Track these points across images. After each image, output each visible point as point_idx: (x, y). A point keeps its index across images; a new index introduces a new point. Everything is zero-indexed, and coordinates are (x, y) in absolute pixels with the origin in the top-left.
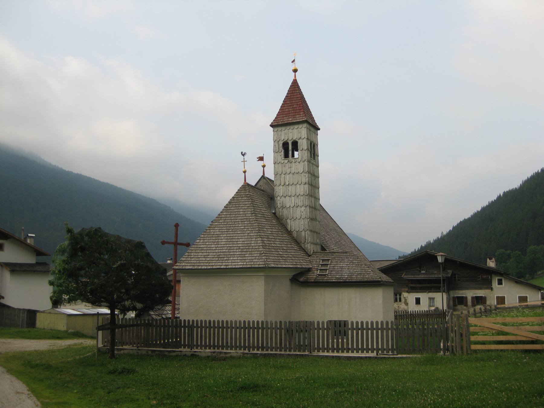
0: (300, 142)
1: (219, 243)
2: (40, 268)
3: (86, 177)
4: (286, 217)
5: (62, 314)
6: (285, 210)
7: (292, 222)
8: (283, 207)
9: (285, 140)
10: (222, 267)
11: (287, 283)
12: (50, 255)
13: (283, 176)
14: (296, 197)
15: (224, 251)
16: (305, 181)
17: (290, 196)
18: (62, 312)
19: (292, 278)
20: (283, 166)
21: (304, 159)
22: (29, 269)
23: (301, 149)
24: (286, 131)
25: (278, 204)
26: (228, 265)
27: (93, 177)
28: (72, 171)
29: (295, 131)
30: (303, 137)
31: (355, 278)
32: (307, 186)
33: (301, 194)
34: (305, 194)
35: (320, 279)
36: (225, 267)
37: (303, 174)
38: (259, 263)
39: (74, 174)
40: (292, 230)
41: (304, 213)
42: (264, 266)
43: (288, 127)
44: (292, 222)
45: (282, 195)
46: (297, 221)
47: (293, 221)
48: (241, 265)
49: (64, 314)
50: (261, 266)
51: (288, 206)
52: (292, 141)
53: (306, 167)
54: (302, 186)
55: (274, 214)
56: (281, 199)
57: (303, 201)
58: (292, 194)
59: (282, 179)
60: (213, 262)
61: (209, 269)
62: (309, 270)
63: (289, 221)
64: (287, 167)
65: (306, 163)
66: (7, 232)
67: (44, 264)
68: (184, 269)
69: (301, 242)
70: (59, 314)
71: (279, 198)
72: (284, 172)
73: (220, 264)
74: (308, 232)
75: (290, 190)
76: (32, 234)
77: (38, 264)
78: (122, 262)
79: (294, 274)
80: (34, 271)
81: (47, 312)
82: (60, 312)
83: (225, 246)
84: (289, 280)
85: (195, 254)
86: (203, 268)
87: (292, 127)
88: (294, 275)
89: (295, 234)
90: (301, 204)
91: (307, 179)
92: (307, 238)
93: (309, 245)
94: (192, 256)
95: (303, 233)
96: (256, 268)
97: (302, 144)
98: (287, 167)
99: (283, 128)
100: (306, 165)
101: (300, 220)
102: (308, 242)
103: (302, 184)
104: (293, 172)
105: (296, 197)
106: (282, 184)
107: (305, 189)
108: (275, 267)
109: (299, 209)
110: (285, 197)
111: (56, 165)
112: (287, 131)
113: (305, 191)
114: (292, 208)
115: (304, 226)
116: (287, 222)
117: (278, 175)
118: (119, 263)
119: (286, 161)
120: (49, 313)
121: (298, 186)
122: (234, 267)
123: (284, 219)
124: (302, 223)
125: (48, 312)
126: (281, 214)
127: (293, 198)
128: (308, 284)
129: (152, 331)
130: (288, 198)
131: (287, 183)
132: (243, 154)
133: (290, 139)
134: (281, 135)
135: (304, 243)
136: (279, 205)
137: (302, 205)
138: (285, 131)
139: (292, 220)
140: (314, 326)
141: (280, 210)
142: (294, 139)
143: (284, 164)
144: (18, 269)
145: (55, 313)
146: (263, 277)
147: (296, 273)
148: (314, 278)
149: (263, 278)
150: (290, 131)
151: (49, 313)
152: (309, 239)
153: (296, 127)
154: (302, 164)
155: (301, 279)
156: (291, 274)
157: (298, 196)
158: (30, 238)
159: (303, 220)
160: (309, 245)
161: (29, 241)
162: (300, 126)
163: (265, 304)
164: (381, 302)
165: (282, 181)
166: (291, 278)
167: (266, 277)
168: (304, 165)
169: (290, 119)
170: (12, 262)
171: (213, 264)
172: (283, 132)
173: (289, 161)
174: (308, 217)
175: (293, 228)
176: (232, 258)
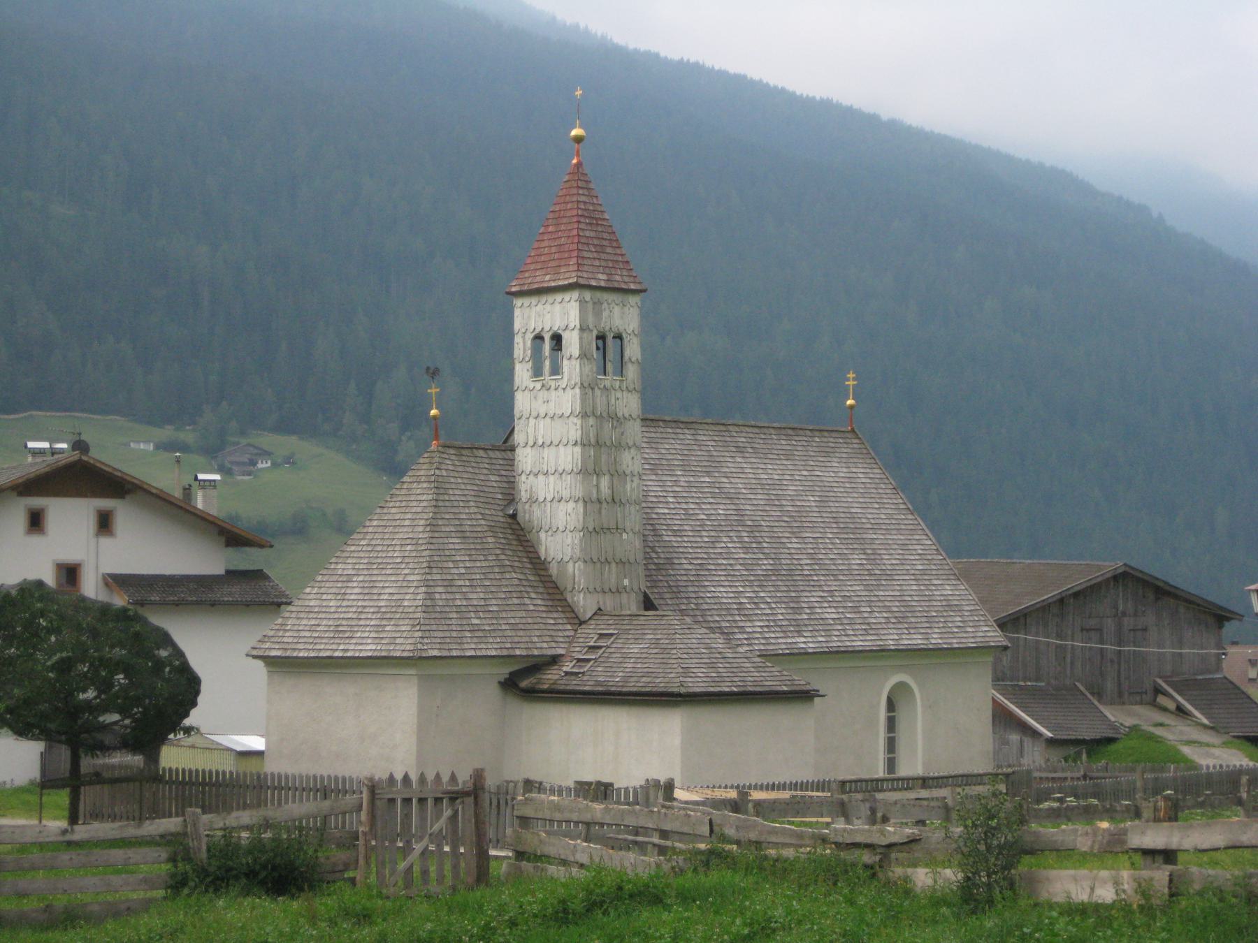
0: (565, 336)
1: (347, 597)
2: (235, 591)
3: (722, 74)
4: (538, 525)
5: (223, 750)
6: (535, 507)
7: (549, 539)
8: (533, 501)
9: (537, 331)
10: (337, 654)
11: (492, 691)
12: (271, 546)
13: (532, 421)
14: (557, 475)
15: (350, 616)
16: (574, 438)
17: (546, 474)
18: (221, 744)
19: (506, 679)
20: (532, 398)
21: (573, 383)
22: (194, 599)
23: (568, 355)
24: (540, 306)
25: (523, 493)
26: (347, 650)
27: (756, 77)
28: (654, 49)
29: (557, 307)
30: (572, 326)
31: (632, 686)
32: (578, 449)
33: (567, 469)
34: (575, 469)
35: (574, 684)
36: (341, 654)
37: (572, 418)
38: (404, 646)
39: (666, 62)
40: (549, 559)
41: (573, 516)
42: (412, 655)
43: (544, 298)
44: (549, 539)
45: (529, 469)
46: (559, 536)
47: (552, 536)
48: (371, 650)
49: (228, 749)
50: (405, 654)
51: (541, 499)
52: (551, 333)
53: (578, 401)
54: (570, 446)
55: (514, 516)
56: (529, 481)
57: (570, 487)
58: (550, 469)
59: (531, 430)
60: (324, 641)
61: (311, 657)
62: (554, 660)
63: (542, 535)
64: (540, 401)
65: (577, 391)
66: (119, 474)
67: (257, 576)
68: (288, 657)
69: (566, 588)
70: (215, 749)
71: (523, 477)
72: (534, 414)
73: (334, 647)
74: (579, 566)
75: (546, 459)
76: (210, 472)
77: (233, 575)
78: (64, 654)
79: (511, 669)
80: (213, 604)
81: (186, 744)
82: (218, 744)
83: (355, 603)
84: (496, 685)
85: (295, 622)
86: (301, 654)
87: (550, 298)
88: (511, 674)
89: (554, 570)
90: (566, 494)
91: (579, 432)
92: (577, 579)
93: (582, 595)
94: (289, 627)
95: (570, 566)
96: (396, 658)
97: (571, 344)
98: (540, 401)
99: (534, 300)
100: (578, 396)
101: (565, 533)
102: (579, 588)
103: (569, 446)
104: (551, 413)
105: (557, 475)
106: (531, 443)
107: (575, 456)
108: (440, 657)
109: (562, 505)
110: (536, 475)
111: (577, 26)
112: (542, 307)
113: (575, 462)
114: (549, 504)
115: (572, 548)
116: (538, 537)
117: (524, 418)
118: (58, 655)
119: (538, 385)
120: (190, 747)
121: (561, 448)
122: (357, 654)
123: (534, 531)
124: (569, 541)
125: (190, 744)
126: (527, 516)
127: (552, 478)
128: (532, 695)
129: (164, 791)
130: (541, 477)
131: (540, 442)
132: (431, 371)
133: (547, 328)
134: (529, 317)
135: (572, 592)
136: (524, 496)
137: (569, 496)
138: (538, 308)
139: (550, 533)
140: (267, 783)
141: (527, 507)
142: (555, 329)
143: (535, 391)
144: (158, 598)
145: (207, 749)
146: (415, 680)
147: (525, 666)
148: (551, 682)
149: (416, 681)
150: (548, 307)
151: (190, 747)
152: (582, 581)
153: (559, 297)
154: (569, 392)
155: (524, 684)
156: (504, 671)
157: (561, 474)
158: (203, 488)
159: (570, 534)
160: (582, 595)
161: (199, 502)
162: (567, 296)
163: (420, 741)
164: (677, 741)
165: (529, 435)
166: (503, 680)
167: (420, 677)
168: (574, 396)
169: (548, 278)
170: (145, 572)
171: (322, 647)
172: (534, 309)
173: (543, 386)
174: (581, 528)
175: (552, 554)
176: (359, 635)
